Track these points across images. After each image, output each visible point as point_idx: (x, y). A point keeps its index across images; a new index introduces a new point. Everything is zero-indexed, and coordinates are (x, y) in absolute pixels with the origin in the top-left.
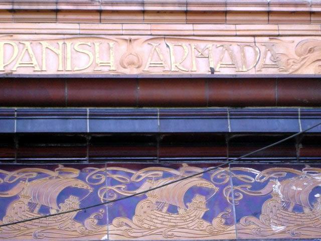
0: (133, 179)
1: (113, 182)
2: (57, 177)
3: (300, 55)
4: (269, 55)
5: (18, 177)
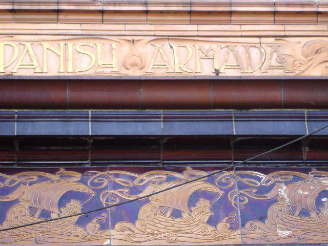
0: (136, 182)
1: (116, 186)
2: (59, 181)
3: (306, 57)
4: (275, 56)
5: (19, 181)
